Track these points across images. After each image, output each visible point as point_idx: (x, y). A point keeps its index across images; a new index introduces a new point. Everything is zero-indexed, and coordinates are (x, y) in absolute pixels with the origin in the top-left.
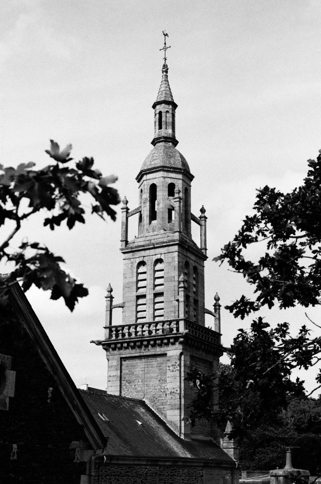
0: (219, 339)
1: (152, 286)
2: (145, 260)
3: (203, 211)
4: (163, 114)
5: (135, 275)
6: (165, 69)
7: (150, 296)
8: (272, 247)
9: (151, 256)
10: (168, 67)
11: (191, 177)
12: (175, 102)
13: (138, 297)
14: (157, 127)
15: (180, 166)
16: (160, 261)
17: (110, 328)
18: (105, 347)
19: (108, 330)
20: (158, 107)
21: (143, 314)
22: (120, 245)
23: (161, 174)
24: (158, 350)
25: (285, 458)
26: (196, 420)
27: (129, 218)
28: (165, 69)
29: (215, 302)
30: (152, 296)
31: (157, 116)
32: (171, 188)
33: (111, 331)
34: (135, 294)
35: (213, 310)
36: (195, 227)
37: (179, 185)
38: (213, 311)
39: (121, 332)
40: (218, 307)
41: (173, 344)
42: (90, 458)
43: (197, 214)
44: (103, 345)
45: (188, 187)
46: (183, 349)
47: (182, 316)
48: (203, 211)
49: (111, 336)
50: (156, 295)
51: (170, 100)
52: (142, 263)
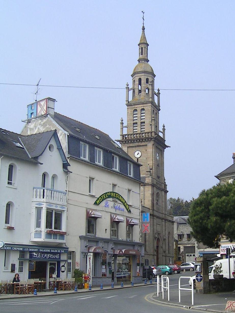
2: (137, 109)
3: (159, 90)
5: (132, 114)
6: (144, 29)
7: (139, 123)
8: (186, 265)
9: (139, 107)
11: (155, 76)
12: (148, 43)
13: (134, 124)
14: (141, 54)
15: (151, 71)
16: (143, 109)
17: (123, 136)
19: (122, 136)
20: (140, 45)
21: (144, 127)
22: (126, 103)
23: (143, 74)
24: (143, 144)
27: (129, 92)
28: (144, 29)
29: (163, 128)
30: (140, 123)
31: (141, 49)
32: (147, 80)
33: (123, 136)
34: (132, 122)
35: (162, 131)
36: (156, 97)
37: (150, 80)
38: (162, 131)
41: (150, 141)
42: (156, 143)
43: (157, 92)
44: (120, 142)
45: (153, 80)
46: (154, 143)
47: (153, 130)
48: (159, 90)
49: (123, 138)
50: (141, 123)
51: (146, 42)
52: (136, 110)
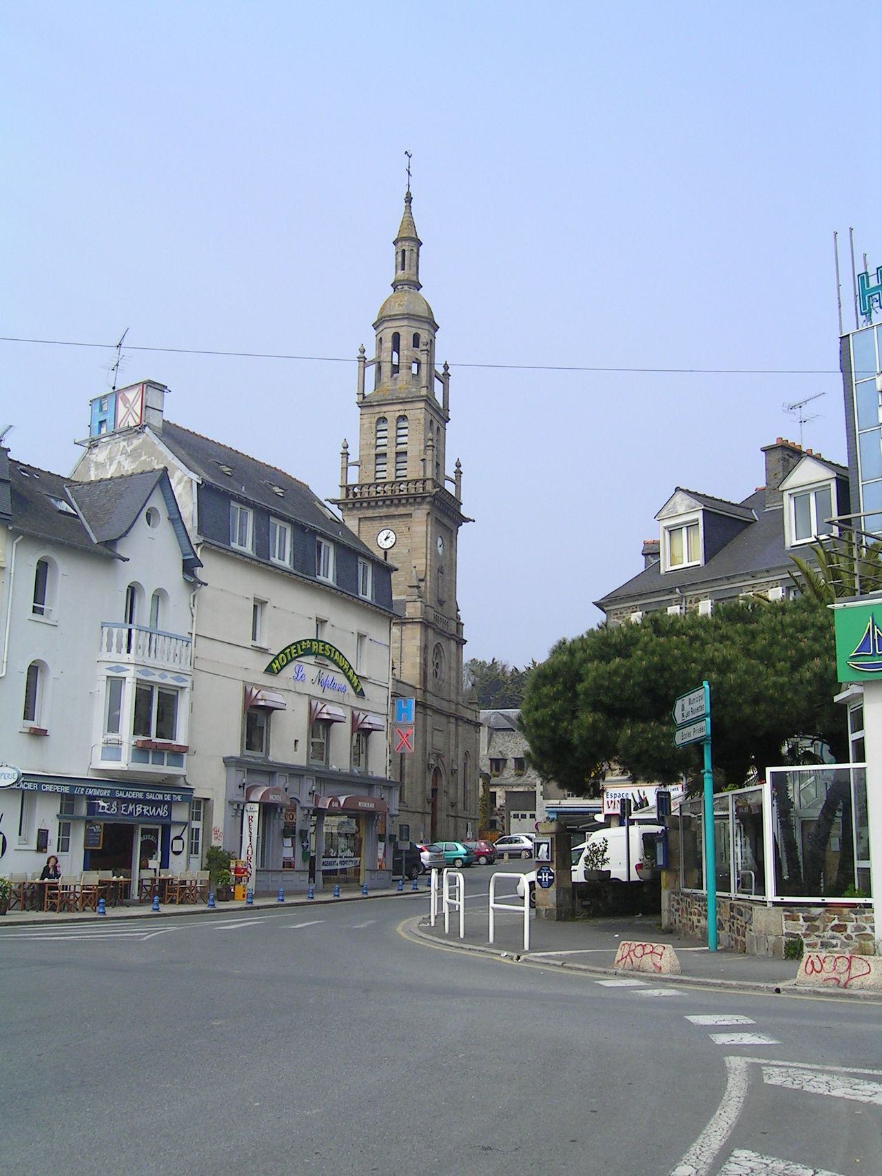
0: (459, 508)
1: (394, 444)
3: (446, 367)
4: (407, 253)
5: (374, 431)
6: (409, 199)
9: (392, 412)
10: (412, 196)
11: (436, 328)
13: (398, 454)
14: (400, 267)
16: (403, 418)
17: (347, 488)
18: (341, 507)
19: (345, 489)
20: (400, 244)
22: (356, 398)
23: (405, 322)
24: (402, 510)
25: (597, 984)
26: (349, 850)
28: (409, 199)
29: (456, 468)
31: (400, 254)
33: (348, 490)
34: (373, 452)
36: (438, 386)
37: (424, 337)
38: (454, 478)
39: (351, 491)
40: (459, 474)
41: (420, 504)
43: (441, 370)
47: (429, 475)
48: (446, 367)
49: (347, 495)
50: (398, 454)
51: (414, 236)
52: (384, 420)
